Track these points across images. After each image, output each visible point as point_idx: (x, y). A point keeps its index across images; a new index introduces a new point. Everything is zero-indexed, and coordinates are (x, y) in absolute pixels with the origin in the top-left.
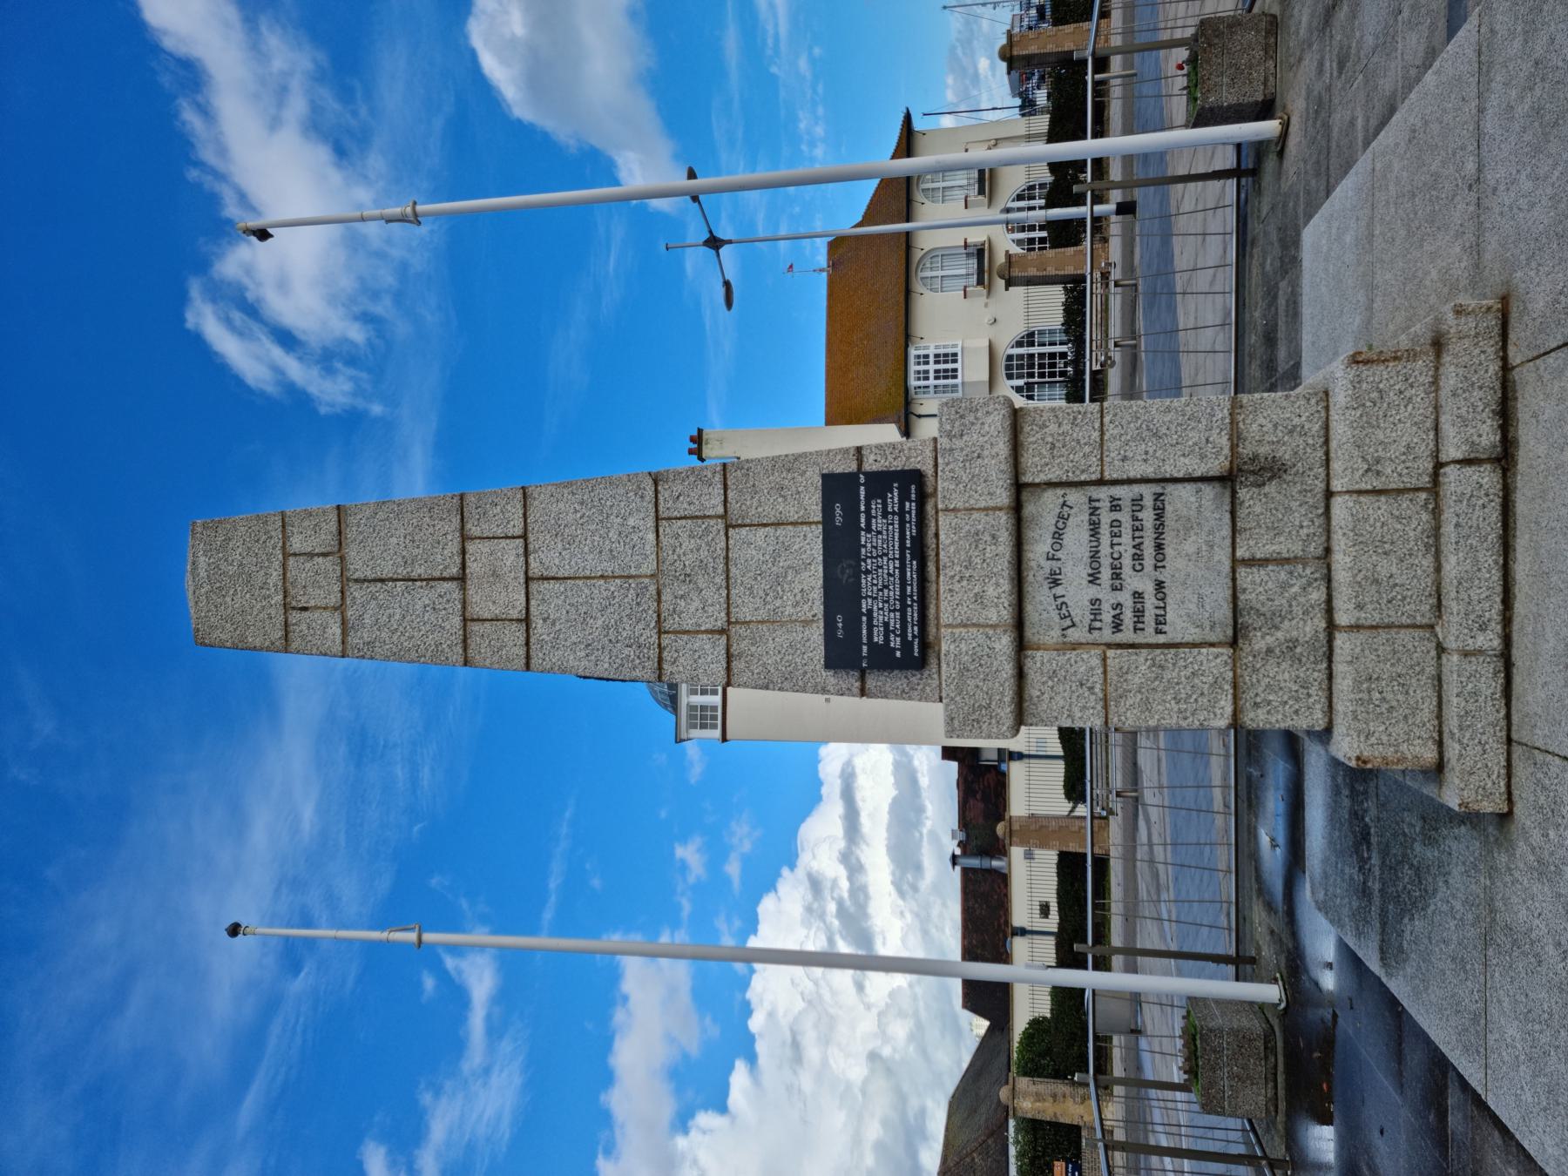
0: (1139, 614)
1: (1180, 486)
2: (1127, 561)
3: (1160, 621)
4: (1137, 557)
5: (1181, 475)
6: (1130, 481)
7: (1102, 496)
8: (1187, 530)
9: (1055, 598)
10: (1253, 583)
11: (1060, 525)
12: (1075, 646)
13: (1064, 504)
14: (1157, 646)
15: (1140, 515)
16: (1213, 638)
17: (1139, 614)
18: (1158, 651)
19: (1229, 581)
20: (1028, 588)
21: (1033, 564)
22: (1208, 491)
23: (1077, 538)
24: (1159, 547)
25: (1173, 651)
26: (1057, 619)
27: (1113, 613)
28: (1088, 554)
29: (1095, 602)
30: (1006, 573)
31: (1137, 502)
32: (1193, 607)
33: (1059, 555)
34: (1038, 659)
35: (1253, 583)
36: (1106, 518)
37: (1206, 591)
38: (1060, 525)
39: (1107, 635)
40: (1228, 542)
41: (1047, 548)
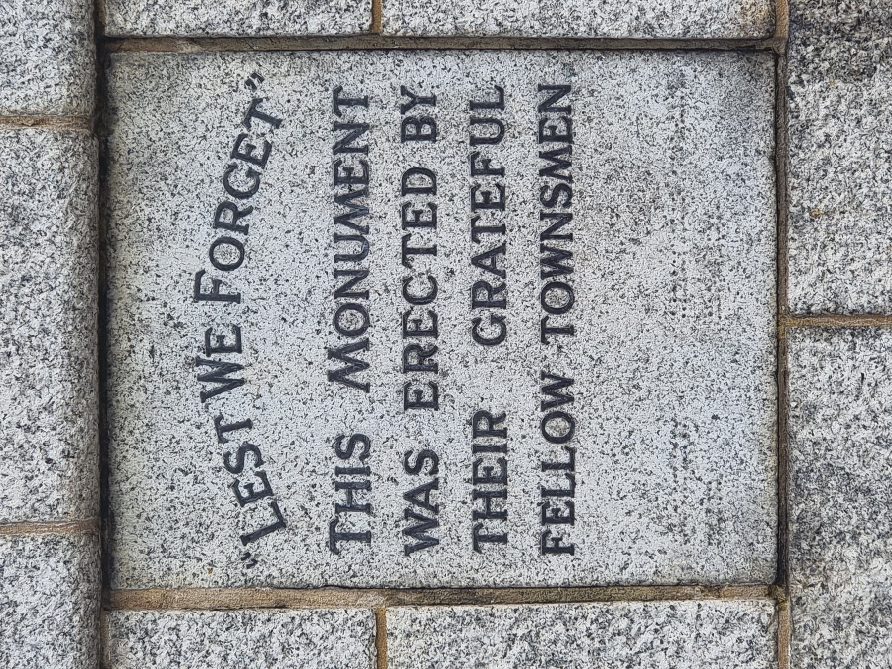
0: (490, 486)
1: (618, 65)
2: (454, 310)
3: (557, 510)
4: (488, 296)
5: (621, 30)
6: (465, 43)
7: (374, 87)
8: (643, 210)
9: (222, 429)
10: (836, 387)
11: (240, 181)
12: (285, 595)
13: (253, 111)
14: (547, 594)
15: (496, 155)
16: (715, 567)
17: (490, 486)
18: (549, 611)
19: (764, 378)
20: (130, 395)
21: (150, 312)
22: (708, 85)
23: (293, 227)
24: (555, 264)
25: (592, 609)
26: (226, 501)
27: (408, 483)
28: (329, 283)
29: (351, 444)
30: (55, 344)
31: (487, 109)
32: (657, 463)
33: (234, 282)
34: (162, 637)
35: (836, 387)
36: (387, 159)
37: (697, 411)
38: (240, 181)
39: (388, 558)
40: (764, 251)
41: (197, 260)
